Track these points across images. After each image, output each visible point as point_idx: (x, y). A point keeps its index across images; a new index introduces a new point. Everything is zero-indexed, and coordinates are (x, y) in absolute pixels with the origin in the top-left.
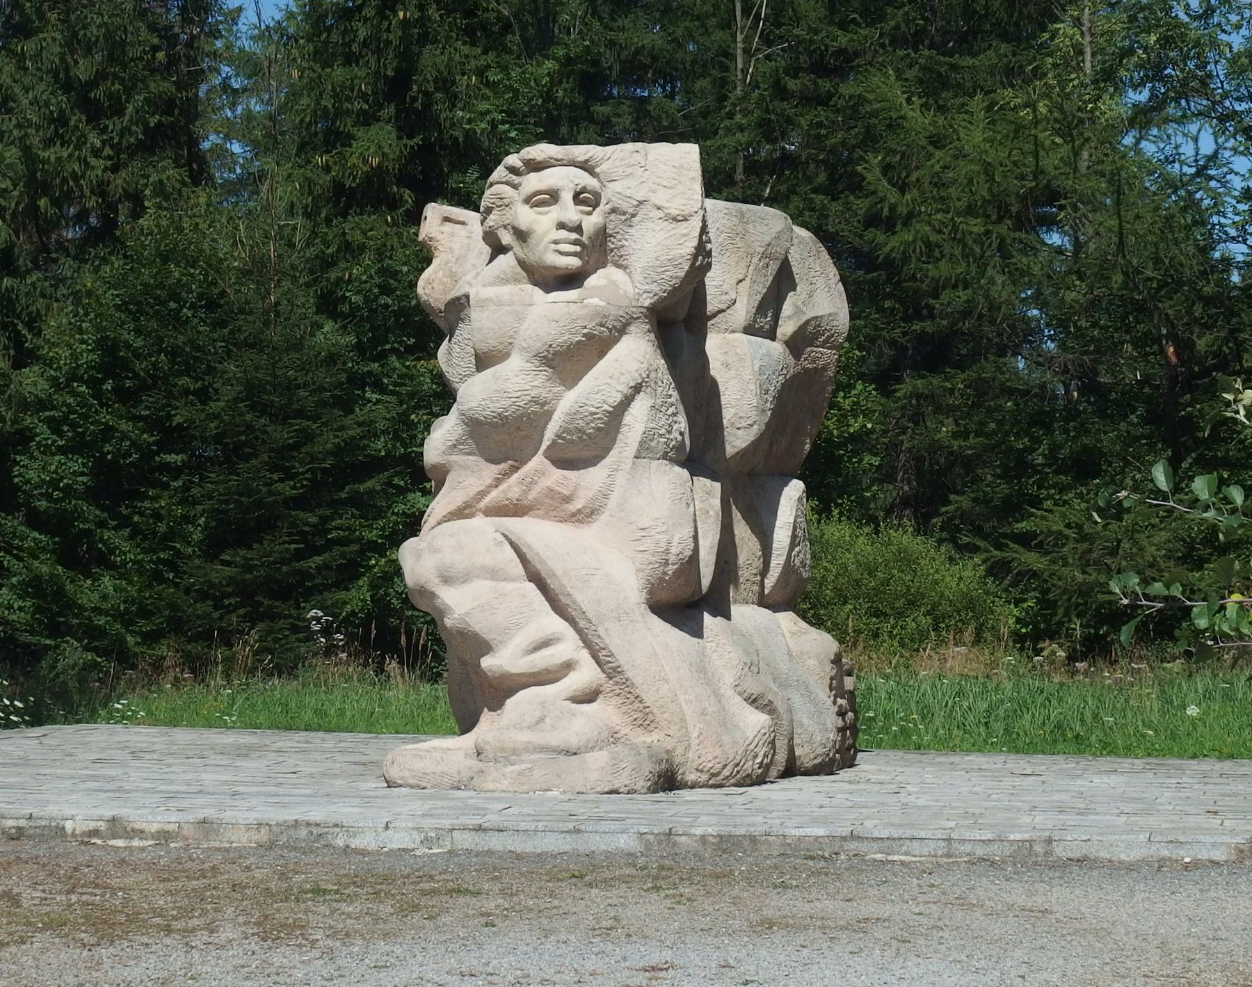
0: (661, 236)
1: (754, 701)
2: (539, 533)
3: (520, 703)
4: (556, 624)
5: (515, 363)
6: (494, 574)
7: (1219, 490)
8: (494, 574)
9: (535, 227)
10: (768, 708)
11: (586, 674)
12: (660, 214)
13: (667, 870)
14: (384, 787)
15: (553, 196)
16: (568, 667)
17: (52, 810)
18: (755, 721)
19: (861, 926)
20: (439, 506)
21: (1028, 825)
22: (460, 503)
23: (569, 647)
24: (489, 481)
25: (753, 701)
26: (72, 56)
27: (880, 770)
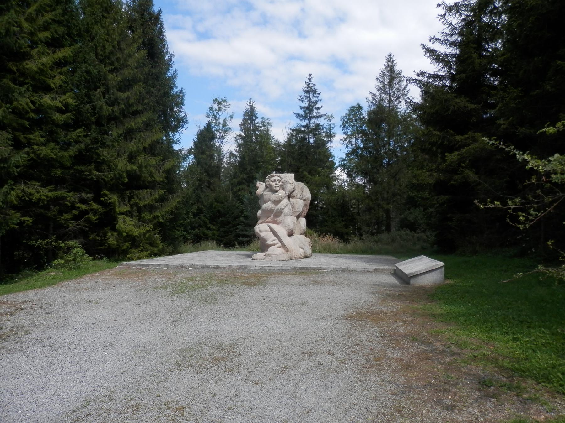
2: (273, 226)
3: (270, 249)
4: (276, 238)
6: (266, 231)
7: (107, 86)
8: (266, 231)
10: (303, 249)
11: (280, 244)
13: (296, 271)
14: (259, 261)
16: (277, 243)
17: (208, 264)
18: (302, 250)
20: (259, 222)
21: (344, 266)
23: (277, 241)
25: (301, 248)
26: (47, 89)
27: (376, 270)
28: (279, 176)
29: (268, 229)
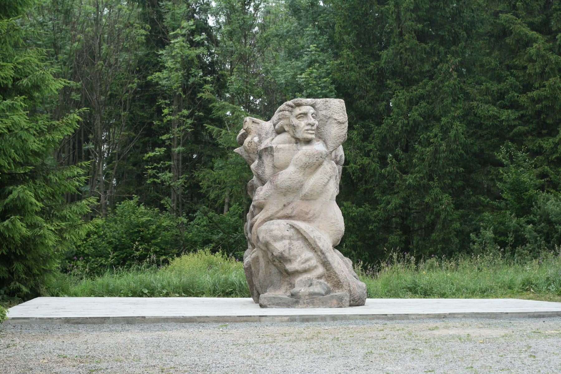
0: (336, 129)
1: (214, 291)
5: (291, 169)
9: (299, 125)
11: (321, 270)
12: (336, 122)
15: (305, 114)
16: (316, 267)
19: (499, 324)
22: (269, 215)
24: (280, 208)
28: (313, 106)
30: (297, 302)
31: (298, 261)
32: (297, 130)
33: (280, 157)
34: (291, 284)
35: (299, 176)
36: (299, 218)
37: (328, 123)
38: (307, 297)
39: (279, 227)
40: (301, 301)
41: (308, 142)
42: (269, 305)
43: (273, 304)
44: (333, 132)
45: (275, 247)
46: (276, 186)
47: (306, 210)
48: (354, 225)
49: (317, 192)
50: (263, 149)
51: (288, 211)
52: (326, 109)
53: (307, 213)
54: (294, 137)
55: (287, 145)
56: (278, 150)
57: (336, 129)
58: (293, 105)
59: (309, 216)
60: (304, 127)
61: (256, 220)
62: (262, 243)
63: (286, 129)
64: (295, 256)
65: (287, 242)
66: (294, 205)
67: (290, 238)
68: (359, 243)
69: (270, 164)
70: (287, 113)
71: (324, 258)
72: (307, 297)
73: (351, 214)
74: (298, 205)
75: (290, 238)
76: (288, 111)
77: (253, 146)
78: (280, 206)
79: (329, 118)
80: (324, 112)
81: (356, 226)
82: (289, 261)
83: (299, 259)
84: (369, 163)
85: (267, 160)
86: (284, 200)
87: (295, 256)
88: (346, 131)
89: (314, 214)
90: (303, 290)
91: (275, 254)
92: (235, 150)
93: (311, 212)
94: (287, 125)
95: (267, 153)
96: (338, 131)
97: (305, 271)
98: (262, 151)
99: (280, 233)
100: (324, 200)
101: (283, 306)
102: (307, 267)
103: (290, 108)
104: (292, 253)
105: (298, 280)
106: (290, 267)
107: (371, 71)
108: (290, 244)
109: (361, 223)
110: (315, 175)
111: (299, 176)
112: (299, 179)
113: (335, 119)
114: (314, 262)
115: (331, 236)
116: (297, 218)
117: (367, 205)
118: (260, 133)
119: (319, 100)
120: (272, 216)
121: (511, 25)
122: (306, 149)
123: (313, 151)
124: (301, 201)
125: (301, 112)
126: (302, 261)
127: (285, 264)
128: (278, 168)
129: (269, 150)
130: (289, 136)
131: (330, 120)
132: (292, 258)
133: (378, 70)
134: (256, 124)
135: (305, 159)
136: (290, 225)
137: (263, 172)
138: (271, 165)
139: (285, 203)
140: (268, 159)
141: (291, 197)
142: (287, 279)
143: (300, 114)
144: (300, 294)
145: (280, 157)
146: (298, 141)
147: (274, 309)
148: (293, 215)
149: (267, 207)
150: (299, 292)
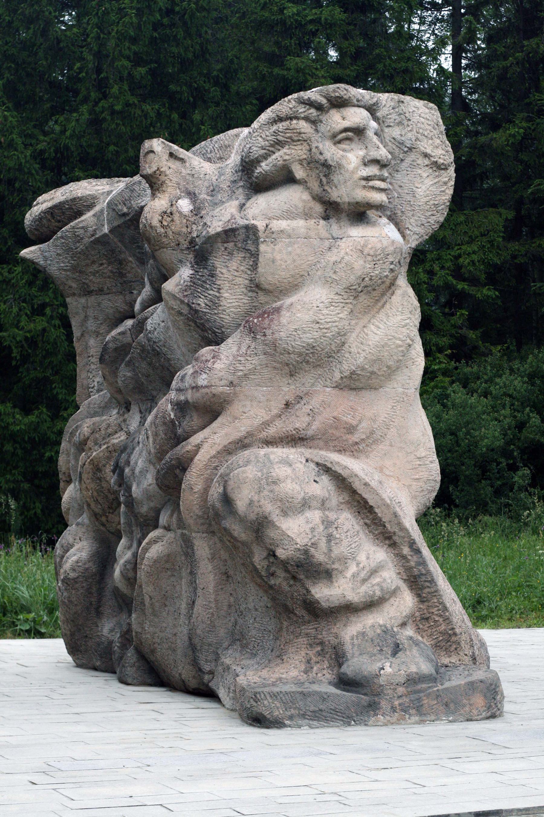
9: (344, 162)
11: (406, 601)
12: (427, 162)
15: (358, 132)
16: (394, 592)
22: (243, 433)
24: (275, 411)
28: (372, 109)
29: (323, 487)
30: (372, 707)
31: (349, 574)
32: (336, 178)
33: (278, 259)
34: (321, 643)
35: (336, 316)
36: (326, 442)
37: (404, 165)
38: (401, 690)
39: (291, 471)
40: (384, 704)
41: (359, 214)
42: (291, 718)
43: (303, 716)
44: (421, 192)
45: (284, 534)
46: (274, 345)
47: (348, 419)
48: (15, 449)
49: (389, 367)
50: (218, 234)
51: (298, 422)
52: (400, 123)
53: (351, 429)
54: (320, 199)
55: (300, 223)
56: (274, 236)
57: (429, 182)
58: (324, 101)
59: (355, 438)
60: (357, 168)
61: (198, 447)
62: (242, 520)
63: (299, 173)
64: (344, 560)
65: (315, 516)
66: (315, 402)
67: (323, 504)
68: (26, 486)
69: (239, 280)
70: (303, 126)
71: (419, 564)
72: (401, 690)
73: (12, 428)
74: (325, 404)
75: (323, 504)
76: (307, 119)
77: (178, 225)
78: (276, 406)
79: (410, 149)
80: (396, 132)
81: (19, 452)
82: (326, 574)
83: (353, 569)
84: (44, 330)
85: (230, 272)
86: (288, 390)
87: (344, 560)
88: (450, 191)
89: (372, 433)
90: (388, 669)
91: (281, 553)
92: (26, 252)
93: (364, 424)
94: (301, 162)
95: (230, 245)
96: (432, 189)
97: (371, 605)
98: (212, 240)
99: (298, 488)
100: (400, 390)
101: (333, 719)
102: (378, 593)
103: (313, 112)
104: (336, 551)
105: (351, 631)
106: (324, 593)
107: (42, 152)
108: (327, 523)
109: (29, 446)
110: (382, 315)
111: (336, 316)
112: (340, 325)
113: (426, 155)
114: (391, 576)
115: (414, 497)
116: (321, 443)
117: (44, 410)
118: (191, 188)
119: (384, 97)
120: (250, 434)
121: (309, 78)
122: (357, 233)
123: (385, 243)
124: (336, 392)
125: (347, 124)
126: (363, 575)
127: (309, 584)
128: (267, 292)
129: (244, 239)
130: (306, 196)
131: (412, 156)
132: (336, 566)
133: (56, 152)
134: (178, 164)
135: (360, 266)
136: (318, 464)
137: (215, 304)
138: (242, 281)
139: (291, 398)
140: (234, 264)
141: (307, 380)
142: (309, 629)
143: (346, 130)
144: (382, 681)
145: (278, 257)
146: (331, 209)
147: (305, 730)
148: (310, 433)
149: (236, 408)
150: (378, 676)
